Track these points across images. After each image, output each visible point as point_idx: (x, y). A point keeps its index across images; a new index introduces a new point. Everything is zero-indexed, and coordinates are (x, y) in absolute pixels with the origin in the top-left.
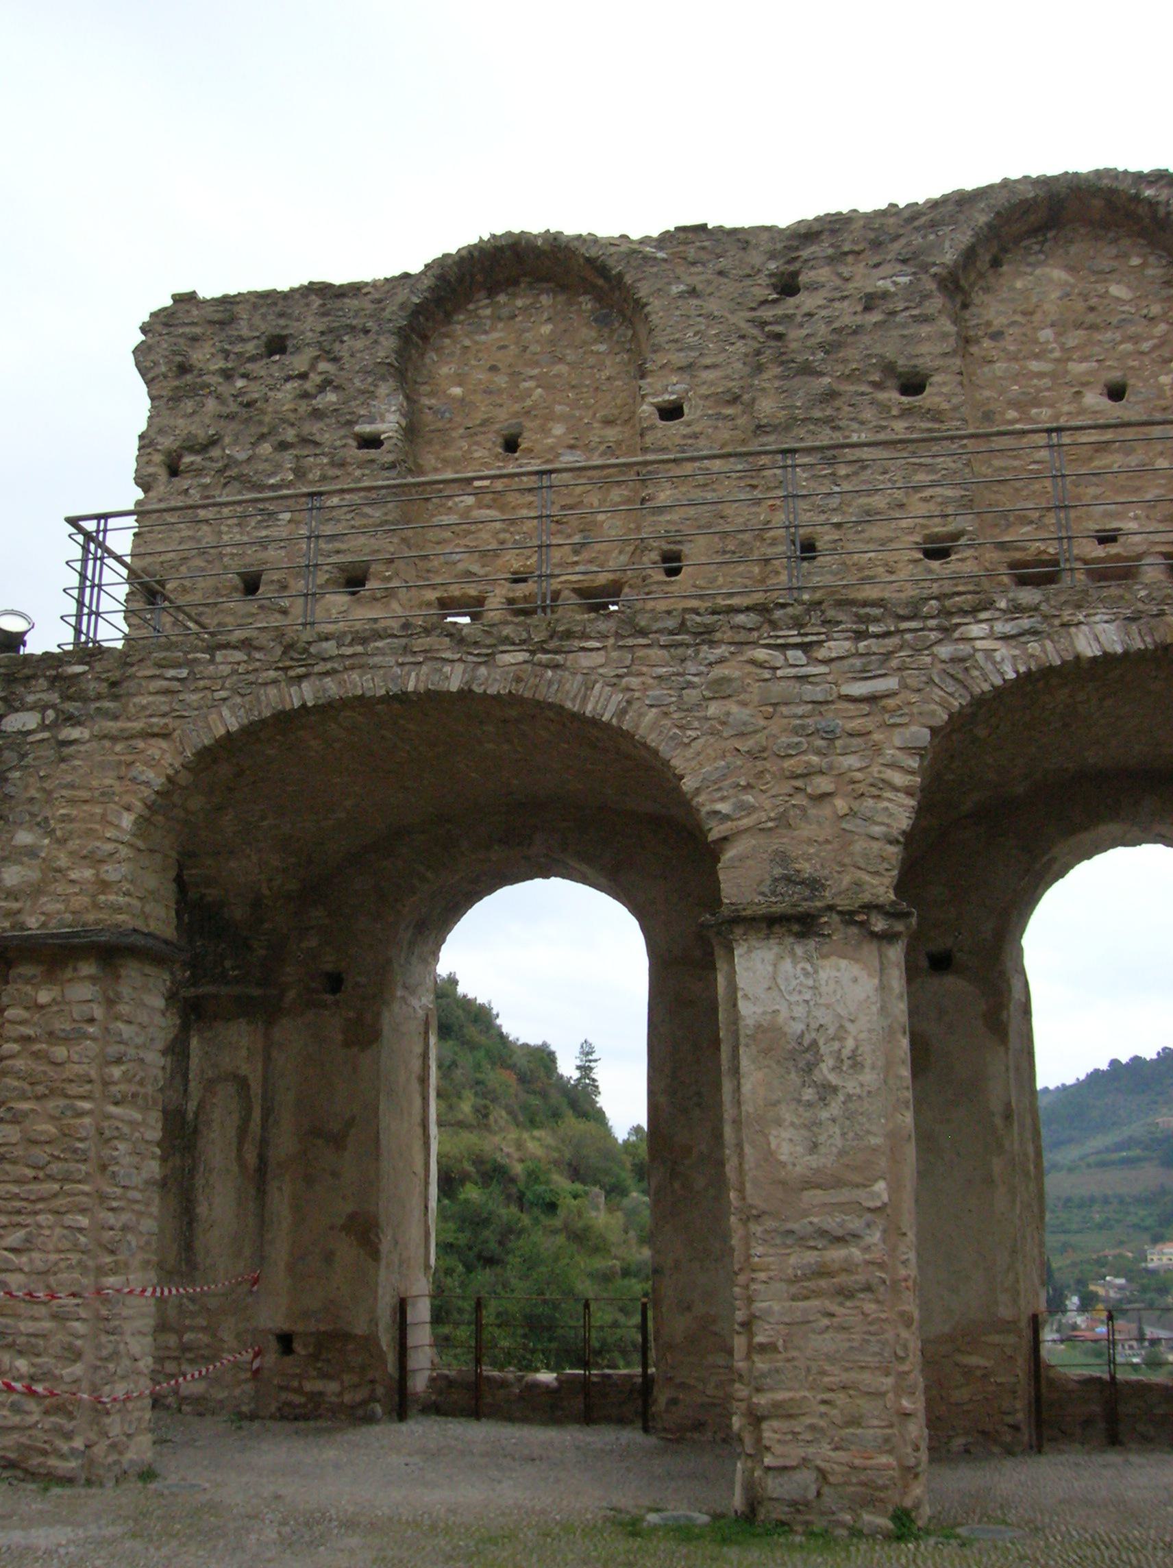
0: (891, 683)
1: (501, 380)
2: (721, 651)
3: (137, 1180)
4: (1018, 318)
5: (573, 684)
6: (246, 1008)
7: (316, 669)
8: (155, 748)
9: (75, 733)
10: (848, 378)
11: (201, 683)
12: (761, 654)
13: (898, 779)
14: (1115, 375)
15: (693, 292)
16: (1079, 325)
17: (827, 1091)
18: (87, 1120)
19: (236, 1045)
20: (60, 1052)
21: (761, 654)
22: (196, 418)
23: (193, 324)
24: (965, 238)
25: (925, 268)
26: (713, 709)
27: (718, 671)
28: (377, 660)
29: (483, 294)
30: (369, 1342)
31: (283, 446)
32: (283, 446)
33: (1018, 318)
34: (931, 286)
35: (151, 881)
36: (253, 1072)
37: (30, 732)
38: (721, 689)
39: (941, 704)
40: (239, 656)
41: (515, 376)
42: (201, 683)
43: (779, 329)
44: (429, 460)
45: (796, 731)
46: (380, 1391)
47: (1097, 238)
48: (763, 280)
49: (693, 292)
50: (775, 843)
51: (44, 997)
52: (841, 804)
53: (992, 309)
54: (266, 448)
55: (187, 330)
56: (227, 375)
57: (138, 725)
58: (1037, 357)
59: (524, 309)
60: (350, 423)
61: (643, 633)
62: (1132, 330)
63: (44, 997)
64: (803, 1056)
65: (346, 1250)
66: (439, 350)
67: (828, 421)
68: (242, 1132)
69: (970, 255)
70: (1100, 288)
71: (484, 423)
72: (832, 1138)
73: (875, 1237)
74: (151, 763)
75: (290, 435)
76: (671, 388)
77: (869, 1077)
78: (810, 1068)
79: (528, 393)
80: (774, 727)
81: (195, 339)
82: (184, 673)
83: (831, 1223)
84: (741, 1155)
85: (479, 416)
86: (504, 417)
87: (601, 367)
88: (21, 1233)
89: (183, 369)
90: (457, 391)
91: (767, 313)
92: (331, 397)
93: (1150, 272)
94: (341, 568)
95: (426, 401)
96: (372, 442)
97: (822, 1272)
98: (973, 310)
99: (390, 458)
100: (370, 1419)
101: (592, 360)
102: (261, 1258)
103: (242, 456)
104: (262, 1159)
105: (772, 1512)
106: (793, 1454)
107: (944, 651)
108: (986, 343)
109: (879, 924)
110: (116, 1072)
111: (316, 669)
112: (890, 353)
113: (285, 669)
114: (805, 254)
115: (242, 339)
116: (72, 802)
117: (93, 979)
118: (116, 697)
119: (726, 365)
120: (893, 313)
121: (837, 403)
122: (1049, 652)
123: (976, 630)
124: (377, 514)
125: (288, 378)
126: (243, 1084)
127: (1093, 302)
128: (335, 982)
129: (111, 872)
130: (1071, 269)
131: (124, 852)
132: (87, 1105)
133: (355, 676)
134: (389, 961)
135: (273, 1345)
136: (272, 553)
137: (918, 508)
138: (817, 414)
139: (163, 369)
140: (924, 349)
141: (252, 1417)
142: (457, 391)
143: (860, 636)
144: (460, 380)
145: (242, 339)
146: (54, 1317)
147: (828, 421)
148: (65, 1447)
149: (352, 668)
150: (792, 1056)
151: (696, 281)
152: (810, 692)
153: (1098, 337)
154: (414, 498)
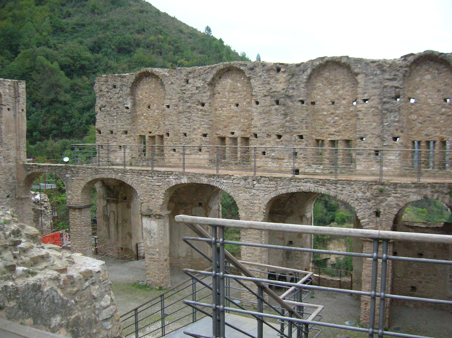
0: (160, 184)
1: (147, 95)
2: (142, 176)
3: (87, 236)
4: (223, 90)
5: (126, 179)
6: (114, 201)
8: (83, 182)
9: (73, 178)
10: (193, 103)
12: (147, 177)
13: (161, 197)
14: (237, 102)
15: (172, 83)
16: (232, 92)
17: (152, 237)
19: (113, 207)
20: (76, 220)
21: (147, 177)
24: (212, 76)
25: (206, 82)
26: (142, 185)
27: (142, 179)
29: (145, 77)
30: (132, 250)
31: (114, 109)
32: (114, 109)
33: (223, 90)
34: (206, 85)
36: (115, 211)
38: (142, 182)
39: (166, 187)
40: (90, 170)
41: (149, 95)
43: (184, 92)
44: (137, 110)
45: (151, 189)
46: (133, 256)
47: (237, 73)
48: (183, 81)
49: (172, 83)
50: (148, 204)
51: (73, 213)
52: (155, 200)
53: (219, 88)
54: (112, 109)
56: (108, 92)
57: (80, 178)
58: (225, 98)
59: (150, 81)
60: (124, 105)
61: (134, 173)
62: (240, 93)
63: (73, 213)
64: (150, 232)
65: (128, 237)
66: (138, 88)
67: (189, 112)
68: (115, 219)
69: (213, 79)
70: (236, 84)
71: (145, 103)
72: (152, 242)
73: (157, 255)
74: (82, 184)
75: (115, 106)
76: (167, 102)
77: (156, 236)
78: (150, 234)
79: (151, 98)
80: (148, 188)
81: (102, 85)
83: (153, 253)
85: (144, 102)
86: (148, 102)
87: (161, 93)
89: (101, 91)
90: (141, 97)
91: (183, 88)
92: (121, 99)
93: (245, 81)
94: (124, 131)
95: (137, 98)
96: (127, 108)
97: (152, 258)
98: (216, 88)
99: (130, 112)
100: (132, 260)
101: (160, 92)
102: (118, 237)
103: (109, 110)
104: (117, 223)
105: (148, 285)
106: (149, 279)
107: (167, 180)
108: (217, 95)
109: (157, 217)
110: (83, 223)
112: (199, 99)
114: (189, 76)
115: (109, 85)
119: (176, 98)
120: (200, 91)
121: (191, 108)
122: (179, 182)
123: (171, 177)
124: (128, 122)
125: (116, 93)
126: (114, 212)
127: (235, 87)
128: (125, 198)
129: (79, 198)
130: (232, 80)
133: (103, 174)
134: (132, 196)
135: (120, 249)
136: (114, 128)
137: (202, 128)
138: (187, 111)
140: (204, 98)
141: (118, 259)
142: (141, 97)
143: (158, 176)
144: (142, 95)
145: (109, 85)
147: (189, 112)
150: (148, 232)
151: (173, 81)
152: (152, 184)
153: (235, 94)
154: (134, 118)
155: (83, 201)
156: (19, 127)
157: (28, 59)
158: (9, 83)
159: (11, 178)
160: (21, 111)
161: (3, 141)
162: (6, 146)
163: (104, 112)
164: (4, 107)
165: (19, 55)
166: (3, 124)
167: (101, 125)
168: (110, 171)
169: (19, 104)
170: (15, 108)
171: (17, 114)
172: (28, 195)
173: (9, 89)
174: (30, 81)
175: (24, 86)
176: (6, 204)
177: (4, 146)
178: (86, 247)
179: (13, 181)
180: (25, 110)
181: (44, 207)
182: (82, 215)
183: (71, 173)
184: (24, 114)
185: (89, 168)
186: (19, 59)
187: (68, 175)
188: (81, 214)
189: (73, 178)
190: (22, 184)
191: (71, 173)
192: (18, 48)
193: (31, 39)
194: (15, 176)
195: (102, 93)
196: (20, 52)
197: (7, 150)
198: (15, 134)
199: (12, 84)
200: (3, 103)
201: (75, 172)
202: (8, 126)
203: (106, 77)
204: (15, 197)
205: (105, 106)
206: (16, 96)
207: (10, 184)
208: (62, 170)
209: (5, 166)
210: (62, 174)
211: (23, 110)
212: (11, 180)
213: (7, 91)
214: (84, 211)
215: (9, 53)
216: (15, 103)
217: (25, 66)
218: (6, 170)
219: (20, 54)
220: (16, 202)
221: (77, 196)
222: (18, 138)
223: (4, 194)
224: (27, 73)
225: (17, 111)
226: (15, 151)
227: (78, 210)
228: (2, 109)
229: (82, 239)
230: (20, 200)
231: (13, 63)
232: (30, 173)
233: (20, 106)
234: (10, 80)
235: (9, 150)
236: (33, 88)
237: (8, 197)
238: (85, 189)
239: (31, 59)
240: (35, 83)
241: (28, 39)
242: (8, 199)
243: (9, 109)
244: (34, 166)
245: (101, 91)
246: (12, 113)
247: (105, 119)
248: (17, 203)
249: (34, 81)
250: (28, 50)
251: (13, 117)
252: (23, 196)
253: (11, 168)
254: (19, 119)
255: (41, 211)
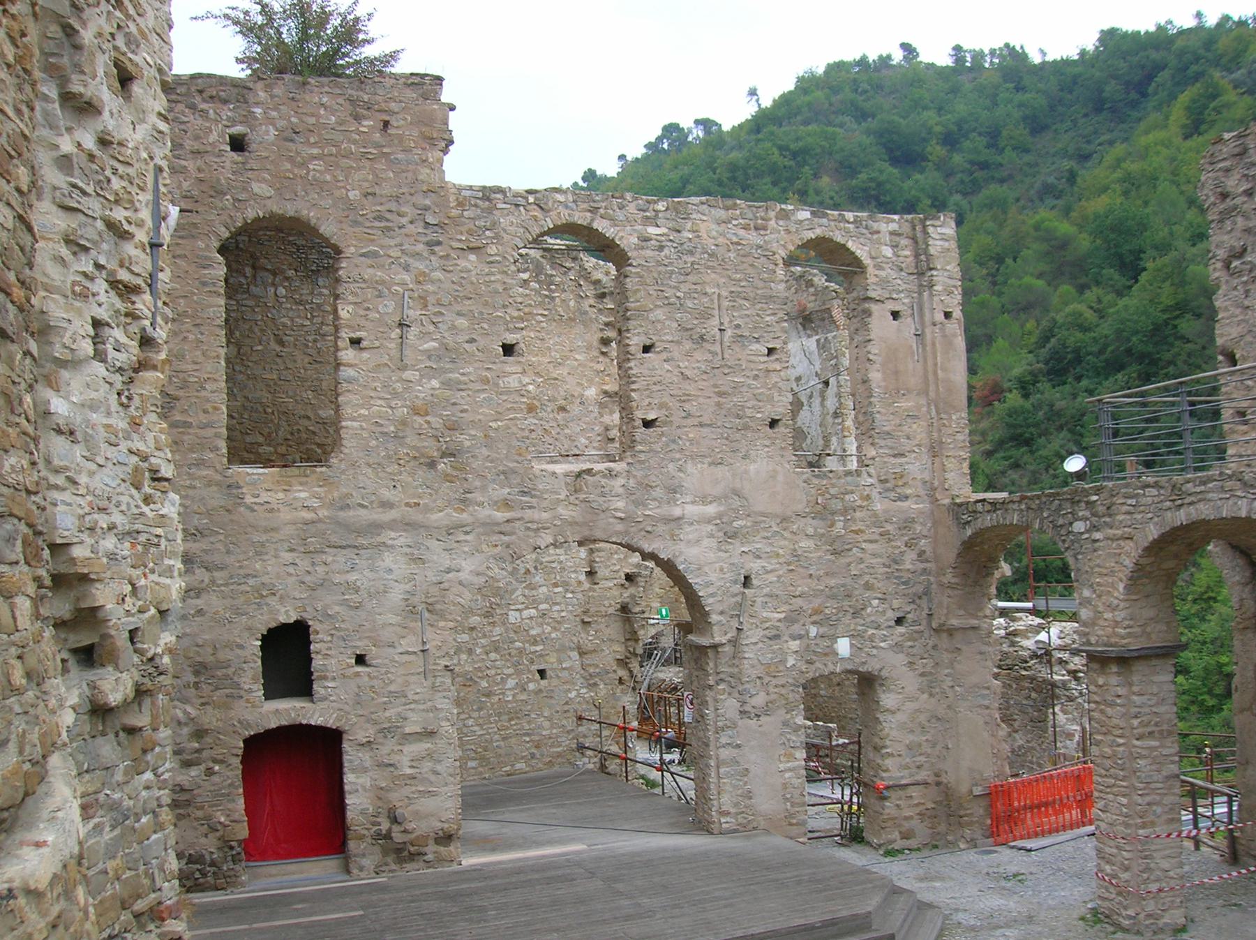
7: (1186, 501)
8: (1128, 546)
9: (1097, 535)
11: (1142, 508)
18: (1121, 749)
20: (1109, 711)
22: (1233, 234)
23: (1224, 159)
28: (1211, 495)
35: (1151, 613)
37: (1082, 533)
40: (1154, 492)
42: (1142, 508)
51: (1101, 681)
55: (1221, 165)
57: (1119, 532)
74: (1128, 555)
81: (1227, 170)
82: (1133, 502)
84: (725, 907)
88: (1103, 802)
89: (1224, 196)
110: (1135, 722)
111: (1186, 501)
113: (1173, 501)
116: (1101, 575)
117: (1119, 674)
118: (1110, 516)
131: (1122, 605)
132: (1121, 741)
133: (1201, 506)
139: (1212, 199)
146: (1117, 847)
148: (1124, 913)
149: (1200, 501)
155: (1137, 630)
156: (935, 373)
157: (1168, 283)
158: (893, 227)
159: (911, 556)
160: (940, 317)
161: (877, 423)
162: (889, 442)
163: (1240, 273)
164: (874, 307)
165: (1144, 277)
166: (877, 366)
167: (1234, 332)
168: (1229, 484)
169: (931, 295)
170: (919, 309)
171: (927, 331)
172: (977, 617)
173: (895, 246)
174: (1177, 343)
175: (949, 229)
176: (891, 647)
177: (882, 443)
178: (1153, 824)
179: (922, 566)
180: (957, 313)
181: (1069, 672)
182: (1135, 689)
183: (1087, 514)
184: (955, 328)
185: (1148, 486)
186: (1144, 286)
187: (1079, 526)
188: (1131, 685)
189: (1097, 535)
190: (949, 577)
191: (1087, 514)
192: (1141, 259)
193: (1175, 228)
194: (929, 550)
195: (1229, 202)
196: (1145, 269)
197: (895, 456)
198: (923, 401)
199: (906, 228)
200: (872, 294)
201: (1101, 509)
202: (896, 373)
203: (1239, 137)
204: (929, 624)
205: (1244, 250)
206: (923, 269)
207: (906, 575)
208: (1060, 507)
209: (886, 511)
210: (1061, 522)
211: (947, 315)
212: (909, 561)
213: (888, 252)
214: (1139, 673)
215: (1116, 277)
216: (920, 294)
217: (1160, 303)
218: (889, 527)
219: (1144, 274)
220: (931, 643)
221: (1114, 609)
222: (934, 413)
223: (884, 612)
224: (1166, 323)
225: (927, 318)
226: (926, 458)
227: (1114, 669)
228: (870, 315)
229: (1136, 789)
230: (945, 635)
231: (1125, 301)
232: (969, 532)
233: (936, 299)
234: (896, 217)
235: (902, 455)
236: (1185, 362)
237: (899, 621)
238: (1138, 576)
239: (1176, 281)
240: (1189, 346)
241: (1166, 229)
242: (901, 629)
243: (895, 315)
244: (979, 507)
245: (1224, 196)
246: (908, 326)
247: (1246, 303)
248: (935, 647)
249: (1188, 341)
250: (1166, 259)
251: (913, 342)
252: (955, 622)
253: (913, 521)
254: (934, 344)
255: (1054, 685)
